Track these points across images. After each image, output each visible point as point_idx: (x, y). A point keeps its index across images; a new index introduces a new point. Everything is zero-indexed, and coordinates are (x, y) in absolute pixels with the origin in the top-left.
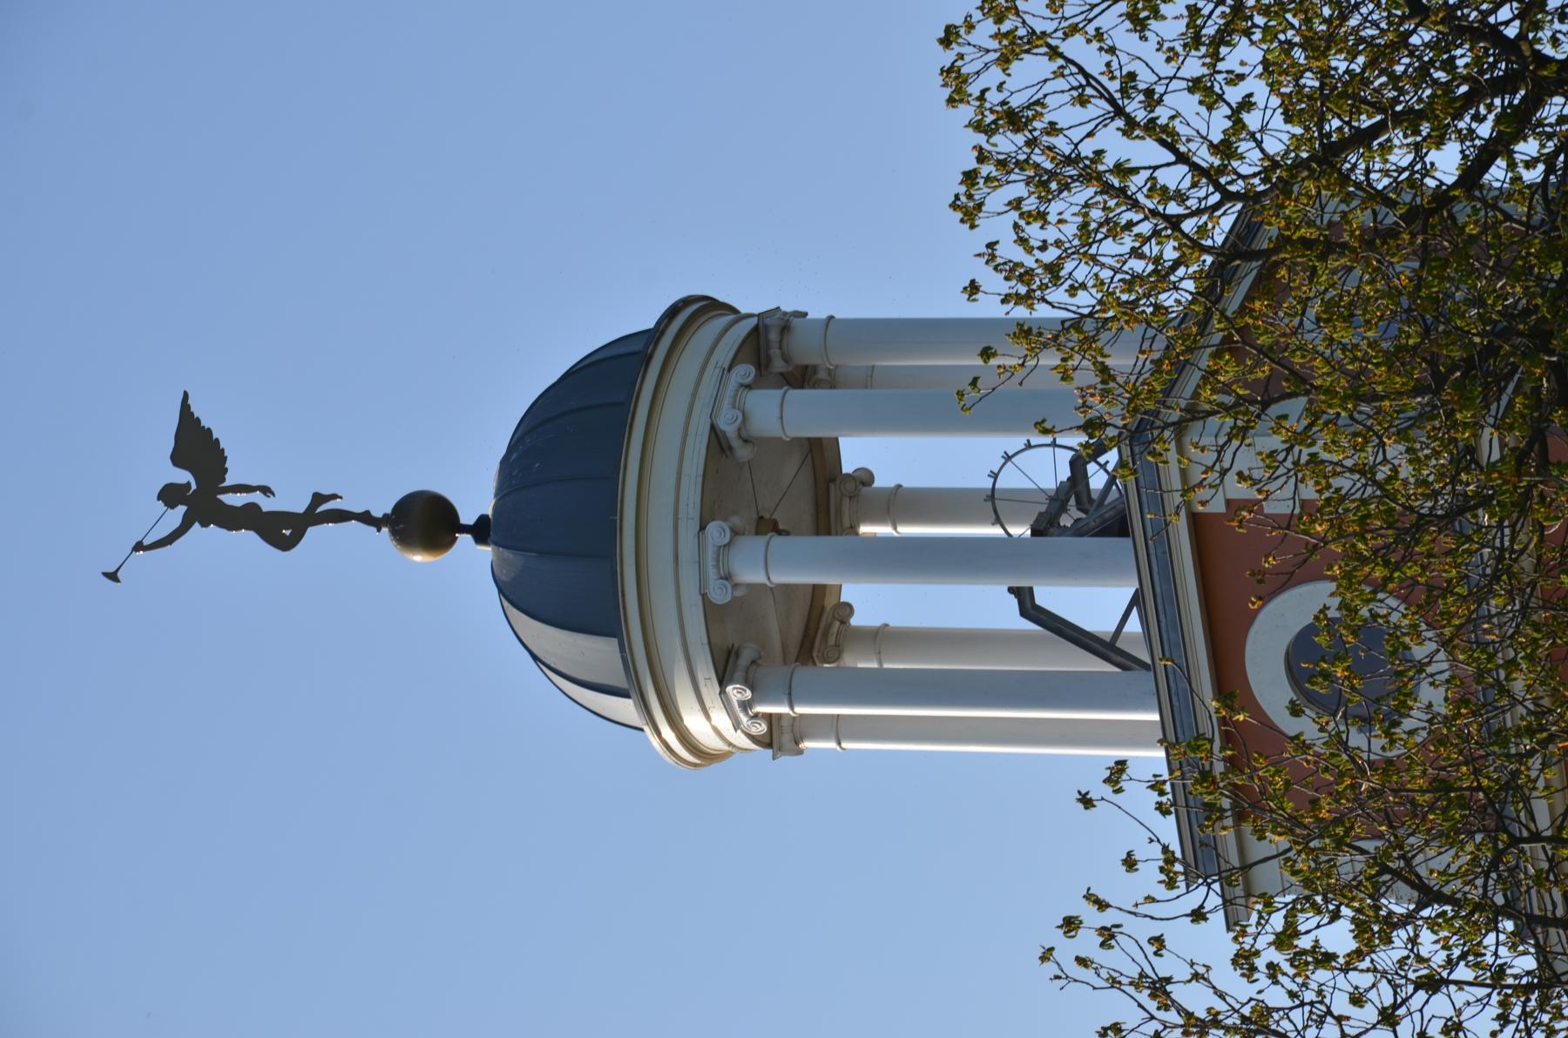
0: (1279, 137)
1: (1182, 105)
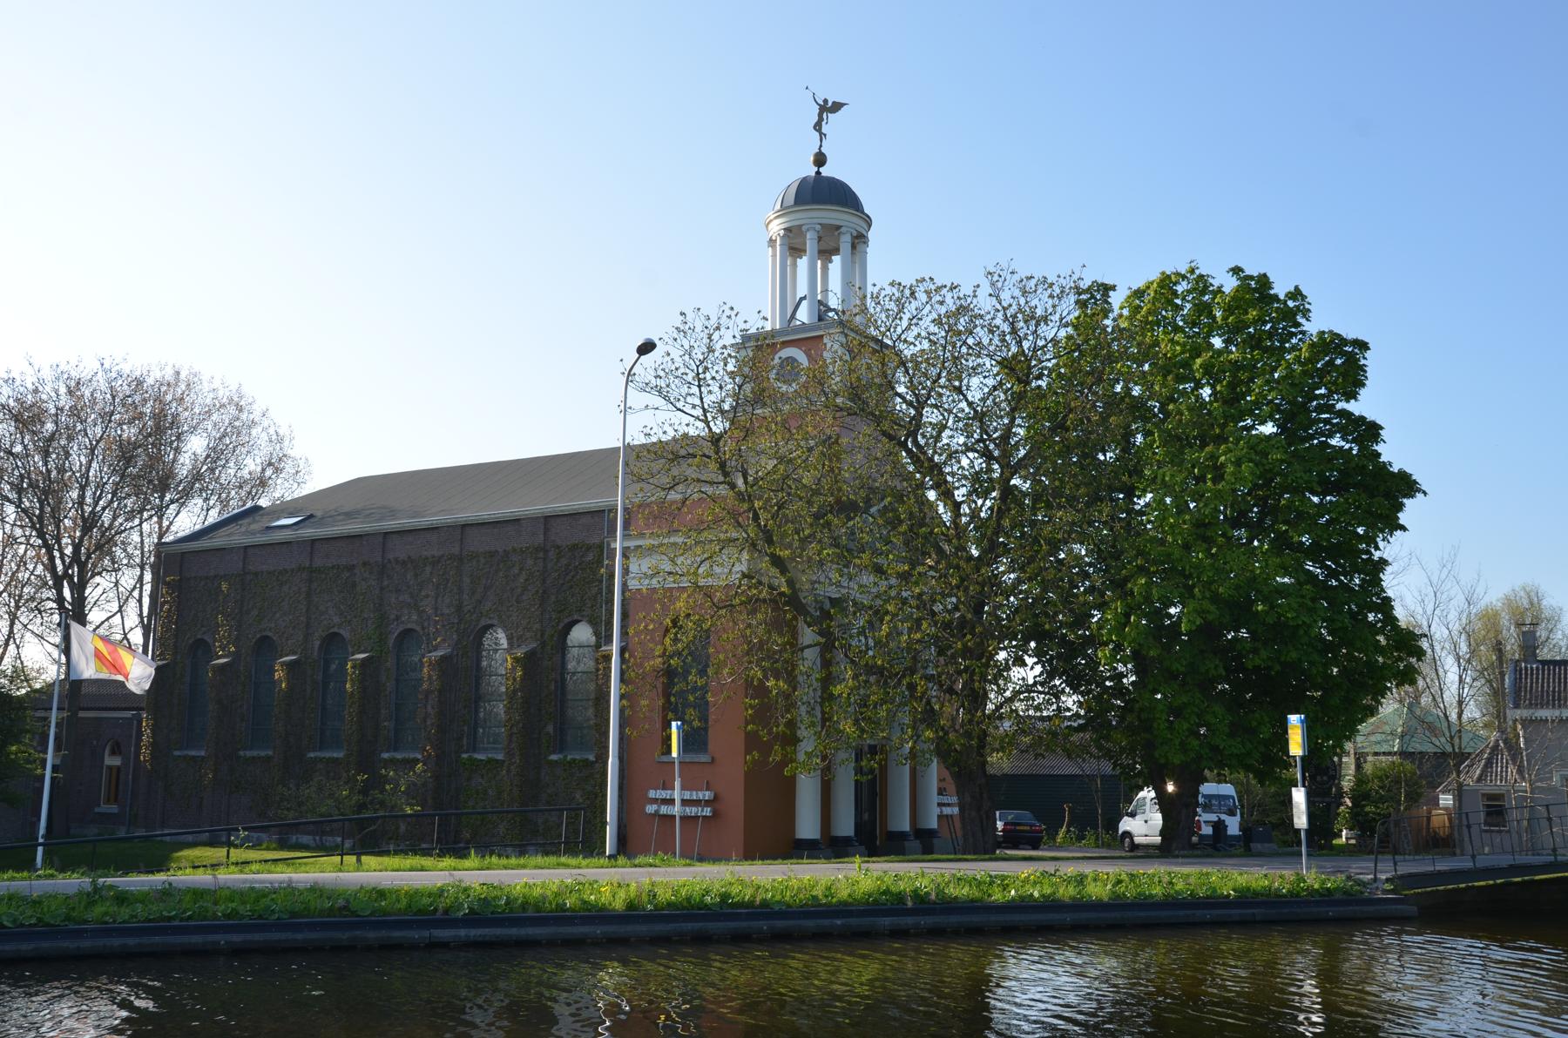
0: (908, 353)
1: (915, 331)
